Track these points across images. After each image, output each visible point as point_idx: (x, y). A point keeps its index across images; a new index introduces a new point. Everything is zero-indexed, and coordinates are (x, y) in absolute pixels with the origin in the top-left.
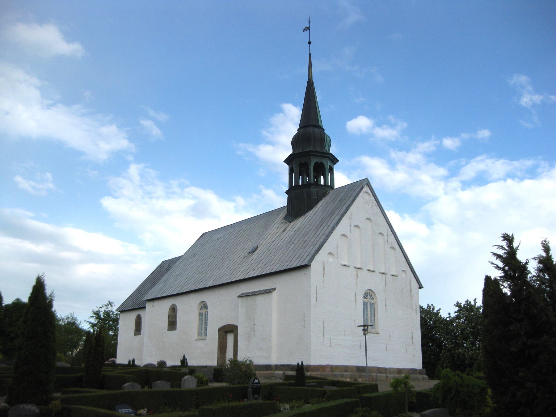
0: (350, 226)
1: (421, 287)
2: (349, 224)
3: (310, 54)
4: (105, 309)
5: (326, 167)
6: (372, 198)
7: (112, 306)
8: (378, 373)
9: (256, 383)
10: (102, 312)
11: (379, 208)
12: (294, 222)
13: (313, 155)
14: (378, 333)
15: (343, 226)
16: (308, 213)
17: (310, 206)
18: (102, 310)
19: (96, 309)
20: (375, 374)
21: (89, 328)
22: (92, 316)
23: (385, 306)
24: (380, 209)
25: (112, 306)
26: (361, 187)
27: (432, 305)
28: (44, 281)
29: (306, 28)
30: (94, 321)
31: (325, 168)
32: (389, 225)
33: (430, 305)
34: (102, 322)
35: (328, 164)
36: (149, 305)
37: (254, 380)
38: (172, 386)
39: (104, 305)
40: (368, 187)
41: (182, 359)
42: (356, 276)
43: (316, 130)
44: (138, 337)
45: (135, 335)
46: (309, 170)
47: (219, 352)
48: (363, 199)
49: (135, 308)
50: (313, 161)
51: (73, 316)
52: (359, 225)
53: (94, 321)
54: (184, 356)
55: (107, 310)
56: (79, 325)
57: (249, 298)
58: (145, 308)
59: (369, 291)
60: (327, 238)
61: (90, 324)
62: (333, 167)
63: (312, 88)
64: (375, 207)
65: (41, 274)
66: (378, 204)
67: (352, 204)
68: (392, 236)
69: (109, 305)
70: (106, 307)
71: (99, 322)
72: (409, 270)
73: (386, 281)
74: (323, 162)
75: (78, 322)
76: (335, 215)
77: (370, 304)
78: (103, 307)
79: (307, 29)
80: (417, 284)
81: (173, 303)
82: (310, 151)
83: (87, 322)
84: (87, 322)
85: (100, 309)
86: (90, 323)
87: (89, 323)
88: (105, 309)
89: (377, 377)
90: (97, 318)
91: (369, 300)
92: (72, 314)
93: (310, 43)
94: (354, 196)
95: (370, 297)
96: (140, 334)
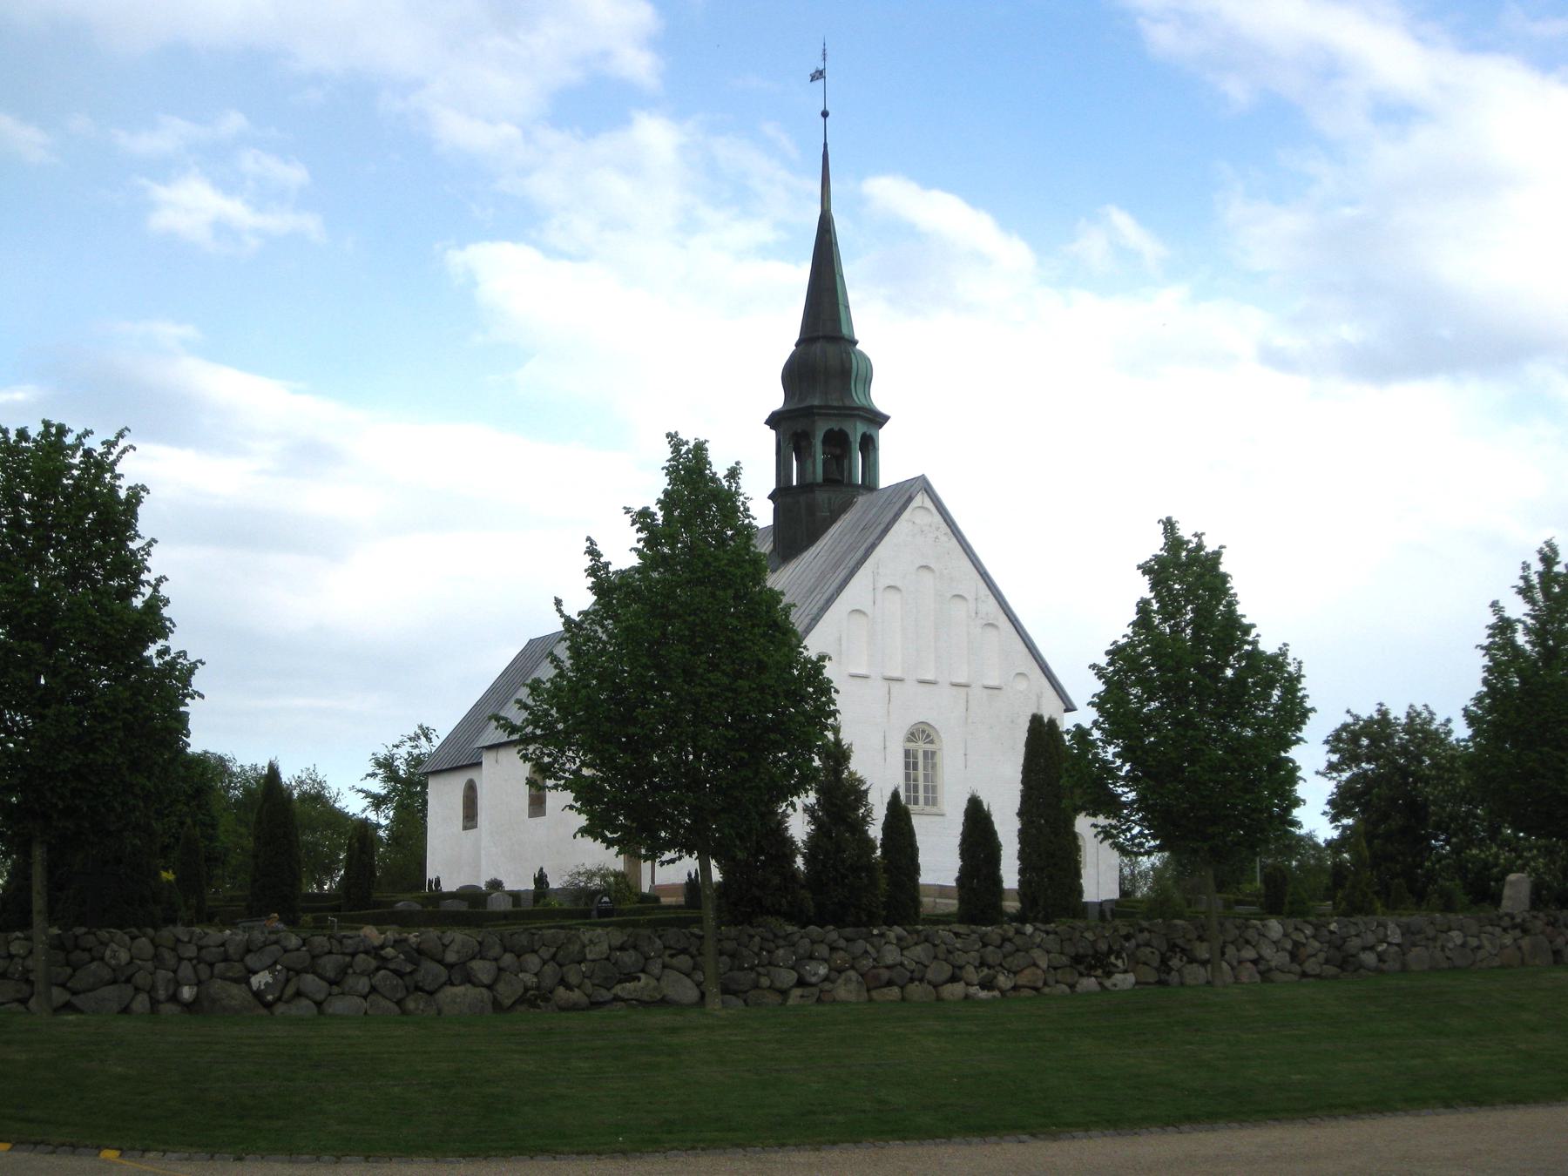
0: (874, 589)
1: (1070, 707)
2: (872, 586)
3: (825, 145)
4: (410, 749)
5: (852, 439)
6: (938, 518)
7: (430, 739)
8: (940, 897)
9: (605, 902)
10: (402, 760)
11: (954, 540)
12: (779, 572)
13: (819, 415)
14: (942, 815)
15: (858, 590)
16: (805, 554)
17: (812, 537)
18: (403, 752)
19: (382, 753)
20: (932, 899)
21: (364, 811)
22: (370, 772)
23: (963, 757)
24: (959, 541)
25: (429, 740)
26: (907, 496)
27: (1426, 706)
28: (278, 768)
29: (816, 72)
30: (377, 786)
31: (851, 442)
32: (981, 575)
33: (1419, 708)
34: (402, 791)
35: (857, 430)
36: (488, 759)
37: (602, 898)
38: (470, 907)
39: (405, 739)
40: (926, 495)
41: (537, 876)
42: (888, 696)
43: (831, 349)
44: (471, 832)
45: (465, 828)
46: (813, 449)
47: (626, 861)
48: (910, 524)
49: (460, 764)
50: (821, 429)
51: (313, 777)
52: (899, 584)
53: (377, 786)
54: (541, 869)
55: (416, 752)
56: (334, 802)
57: (1030, 657)
58: (481, 763)
59: (923, 727)
60: (813, 623)
61: (366, 797)
62: (875, 437)
63: (827, 236)
64: (944, 539)
65: (273, 759)
66: (952, 531)
67: (880, 543)
68: (992, 600)
69: (422, 737)
70: (414, 744)
71: (393, 791)
72: (1038, 671)
73: (967, 702)
74: (846, 430)
75: (329, 793)
76: (842, 567)
77: (925, 753)
78: (403, 742)
79: (819, 75)
80: (1061, 702)
81: (470, 777)
82: (812, 407)
83: (359, 791)
84: (359, 791)
85: (395, 750)
86: (368, 794)
87: (364, 794)
88: (410, 749)
89: (935, 907)
90: (387, 779)
91: (920, 747)
92: (311, 771)
93: (825, 114)
94: (888, 520)
95: (926, 738)
96: (475, 826)
